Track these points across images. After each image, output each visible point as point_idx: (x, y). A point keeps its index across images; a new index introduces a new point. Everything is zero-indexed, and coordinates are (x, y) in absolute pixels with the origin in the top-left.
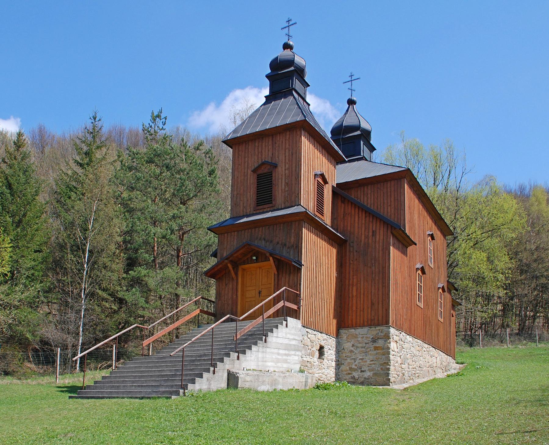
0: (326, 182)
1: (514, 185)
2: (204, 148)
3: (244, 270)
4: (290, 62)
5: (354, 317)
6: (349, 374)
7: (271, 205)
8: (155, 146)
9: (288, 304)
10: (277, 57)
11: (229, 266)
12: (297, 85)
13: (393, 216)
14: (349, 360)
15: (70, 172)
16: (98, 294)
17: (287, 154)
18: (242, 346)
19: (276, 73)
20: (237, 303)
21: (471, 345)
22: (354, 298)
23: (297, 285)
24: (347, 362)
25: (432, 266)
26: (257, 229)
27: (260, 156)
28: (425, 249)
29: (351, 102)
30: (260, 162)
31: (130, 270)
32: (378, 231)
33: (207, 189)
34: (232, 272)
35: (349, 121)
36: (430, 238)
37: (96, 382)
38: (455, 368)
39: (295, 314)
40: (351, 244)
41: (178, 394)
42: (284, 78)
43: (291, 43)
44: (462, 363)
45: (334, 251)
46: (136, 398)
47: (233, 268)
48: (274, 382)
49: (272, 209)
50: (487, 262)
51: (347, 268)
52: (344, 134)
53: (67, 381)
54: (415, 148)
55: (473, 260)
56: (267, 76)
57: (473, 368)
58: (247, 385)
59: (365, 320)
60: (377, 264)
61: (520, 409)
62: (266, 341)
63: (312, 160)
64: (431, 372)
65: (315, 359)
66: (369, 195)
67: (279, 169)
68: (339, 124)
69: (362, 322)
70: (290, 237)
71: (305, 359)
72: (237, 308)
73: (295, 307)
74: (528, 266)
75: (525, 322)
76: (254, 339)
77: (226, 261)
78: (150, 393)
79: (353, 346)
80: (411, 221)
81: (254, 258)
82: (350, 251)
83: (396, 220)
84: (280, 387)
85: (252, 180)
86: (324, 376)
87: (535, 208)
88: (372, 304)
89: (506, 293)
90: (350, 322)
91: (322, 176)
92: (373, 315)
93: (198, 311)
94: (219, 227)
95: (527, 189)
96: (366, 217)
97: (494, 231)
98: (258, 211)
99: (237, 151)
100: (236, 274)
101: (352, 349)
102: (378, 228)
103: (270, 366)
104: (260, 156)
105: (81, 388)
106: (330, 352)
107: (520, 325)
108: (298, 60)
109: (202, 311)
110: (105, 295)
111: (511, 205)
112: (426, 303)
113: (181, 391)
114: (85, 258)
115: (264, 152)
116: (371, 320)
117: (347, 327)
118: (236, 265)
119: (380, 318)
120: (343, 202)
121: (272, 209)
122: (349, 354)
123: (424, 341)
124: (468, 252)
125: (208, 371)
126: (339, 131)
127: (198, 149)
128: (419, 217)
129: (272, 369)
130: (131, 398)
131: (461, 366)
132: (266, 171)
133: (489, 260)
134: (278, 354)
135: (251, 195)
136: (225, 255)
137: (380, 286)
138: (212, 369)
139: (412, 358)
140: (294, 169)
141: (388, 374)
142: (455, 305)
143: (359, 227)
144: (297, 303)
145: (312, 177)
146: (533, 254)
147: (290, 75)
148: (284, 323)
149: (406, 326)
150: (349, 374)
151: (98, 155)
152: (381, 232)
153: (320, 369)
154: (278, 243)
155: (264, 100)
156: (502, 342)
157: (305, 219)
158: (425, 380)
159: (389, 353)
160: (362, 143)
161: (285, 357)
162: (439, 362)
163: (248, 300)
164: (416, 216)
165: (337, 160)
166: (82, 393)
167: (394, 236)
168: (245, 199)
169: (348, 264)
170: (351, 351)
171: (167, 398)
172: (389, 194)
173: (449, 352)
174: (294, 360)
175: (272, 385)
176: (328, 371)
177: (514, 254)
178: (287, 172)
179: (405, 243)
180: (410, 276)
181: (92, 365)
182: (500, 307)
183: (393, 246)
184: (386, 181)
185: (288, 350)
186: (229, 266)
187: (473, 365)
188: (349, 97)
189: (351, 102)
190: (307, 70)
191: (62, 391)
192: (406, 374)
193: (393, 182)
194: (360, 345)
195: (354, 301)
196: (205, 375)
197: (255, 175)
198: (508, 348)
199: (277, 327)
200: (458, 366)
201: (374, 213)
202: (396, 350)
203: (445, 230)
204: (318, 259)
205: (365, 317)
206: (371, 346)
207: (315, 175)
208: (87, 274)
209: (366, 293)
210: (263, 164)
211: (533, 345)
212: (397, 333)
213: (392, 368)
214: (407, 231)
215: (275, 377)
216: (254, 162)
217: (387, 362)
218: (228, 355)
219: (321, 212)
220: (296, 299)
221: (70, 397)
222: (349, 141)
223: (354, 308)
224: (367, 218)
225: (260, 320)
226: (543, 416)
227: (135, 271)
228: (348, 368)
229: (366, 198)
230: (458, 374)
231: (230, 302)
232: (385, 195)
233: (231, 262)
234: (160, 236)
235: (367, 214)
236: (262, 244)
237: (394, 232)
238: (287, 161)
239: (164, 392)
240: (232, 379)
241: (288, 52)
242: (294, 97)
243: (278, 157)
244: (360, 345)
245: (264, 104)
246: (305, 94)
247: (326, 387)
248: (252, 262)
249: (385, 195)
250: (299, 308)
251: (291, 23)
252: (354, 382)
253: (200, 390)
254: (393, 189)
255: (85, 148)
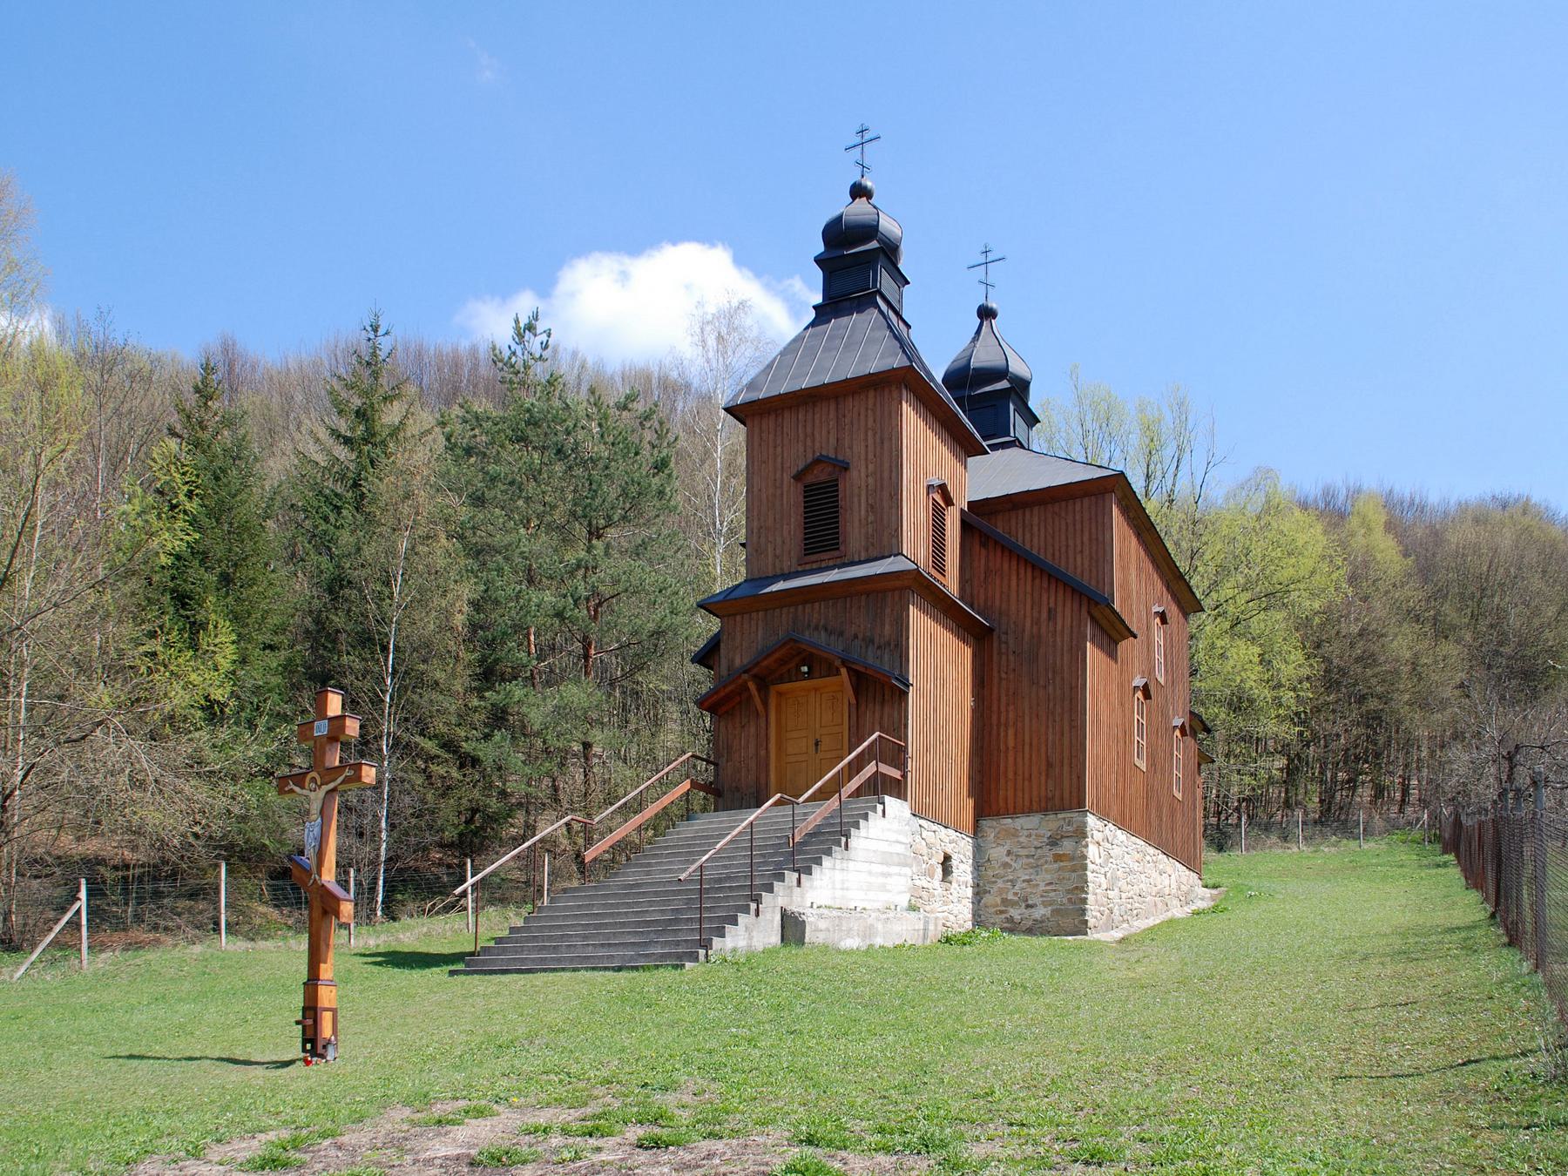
0: (949, 501)
1: (1311, 487)
2: (640, 407)
3: (780, 694)
4: (869, 230)
5: (1010, 793)
6: (1002, 912)
7: (836, 553)
8: (529, 401)
9: (886, 769)
10: (840, 217)
11: (752, 686)
12: (886, 282)
13: (1086, 575)
14: (1000, 884)
15: (321, 459)
16: (417, 745)
17: (870, 441)
18: (802, 855)
19: (837, 253)
20: (767, 765)
21: (1220, 849)
22: (1011, 753)
23: (900, 728)
24: (995, 888)
25: (1162, 680)
26: (808, 606)
27: (809, 443)
28: (1149, 643)
29: (986, 313)
30: (810, 460)
31: (488, 689)
32: (1059, 609)
33: (650, 506)
34: (757, 700)
35: (984, 358)
36: (1158, 620)
37: (499, 940)
38: (1203, 898)
39: (898, 788)
40: (1003, 638)
41: (696, 959)
42: (855, 265)
43: (869, 184)
44: (1215, 887)
45: (968, 652)
46: (606, 969)
47: (759, 690)
48: (869, 931)
49: (839, 561)
50: (1257, 662)
51: (995, 690)
52: (972, 388)
53: (372, 942)
54: (1103, 407)
55: (1231, 662)
56: (818, 260)
57: (1241, 897)
58: (820, 938)
59: (1035, 799)
60: (1058, 679)
61: (1373, 969)
62: (847, 848)
63: (922, 452)
64: (1160, 905)
65: (937, 881)
66: (1035, 529)
67: (854, 473)
68: (963, 362)
69: (1027, 803)
70: (883, 625)
71: (918, 883)
72: (767, 776)
73: (896, 774)
74: (1343, 672)
75: (1333, 797)
76: (822, 842)
77: (745, 676)
78: (632, 958)
79: (1009, 853)
80: (1125, 584)
81: (805, 669)
82: (1000, 653)
83: (1093, 583)
84: (878, 941)
85: (793, 497)
86: (952, 918)
87: (1359, 541)
88: (1049, 765)
89: (1301, 734)
90: (1001, 803)
91: (943, 489)
92: (1050, 787)
93: (686, 785)
94: (724, 600)
95: (1341, 498)
96: (1033, 579)
97: (1272, 598)
98: (808, 567)
99: (757, 430)
100: (765, 704)
101: (1008, 859)
102: (1060, 603)
103: (856, 899)
104: (809, 443)
105: (472, 954)
106: (962, 867)
107: (1321, 801)
108: (887, 225)
109: (694, 784)
110: (430, 746)
111: (1313, 537)
112: (1152, 763)
113: (702, 952)
114: (386, 660)
115: (821, 433)
116: (1048, 799)
117: (998, 814)
118: (764, 683)
119: (1066, 795)
120: (983, 545)
121: (839, 561)
122: (1001, 871)
123: (1148, 840)
124: (1219, 643)
125: (746, 910)
126: (961, 377)
127: (625, 408)
128: (1138, 575)
129: (860, 905)
130: (593, 969)
131: (1214, 892)
132: (823, 478)
133: (1264, 661)
134: (870, 873)
135: (791, 530)
136: (737, 662)
137: (1066, 728)
138: (753, 906)
139: (1131, 877)
140: (886, 474)
141: (1084, 911)
142: (1204, 758)
143: (1018, 598)
144: (901, 764)
145: (923, 491)
146: (1352, 645)
147: (869, 259)
148: (880, 807)
149: (1115, 810)
150: (1002, 912)
151: (390, 415)
152: (1067, 612)
153: (945, 903)
154: (856, 636)
155: (812, 315)
156: (1285, 839)
157: (918, 586)
158: (1151, 922)
159: (1085, 868)
160: (1012, 407)
161: (881, 880)
162: (1174, 885)
163: (792, 759)
164: (1133, 573)
165: (966, 447)
166: (476, 963)
167: (1093, 619)
168: (779, 540)
169: (996, 681)
170: (1006, 865)
171: (676, 967)
172: (1078, 526)
173: (1192, 863)
174: (898, 890)
175: (864, 938)
176: (960, 907)
177: (1315, 646)
178: (871, 480)
179: (1113, 632)
180: (1122, 705)
181: (411, 906)
182: (1281, 762)
183: (1093, 642)
184: (1074, 498)
185: (887, 864)
186: (752, 686)
187: (1238, 889)
188: (982, 301)
189: (986, 313)
190: (903, 247)
191: (379, 964)
192: (1116, 911)
193: (1086, 501)
194: (1023, 852)
195: (1011, 759)
196: (742, 918)
197: (800, 487)
198: (1298, 851)
199: (866, 817)
200: (1208, 892)
201: (1053, 568)
202: (1098, 861)
203: (1188, 603)
204: (937, 666)
205: (1035, 793)
206: (1049, 854)
207: (929, 487)
208: (392, 699)
209: (1035, 742)
210: (818, 461)
211: (1353, 844)
212: (1100, 824)
213: (1091, 897)
214: (1116, 606)
215: (870, 921)
216: (796, 456)
217: (1081, 887)
218: (781, 878)
219: (941, 570)
220: (898, 756)
221: (452, 973)
222: (985, 404)
223: (1011, 775)
224: (1037, 581)
225: (833, 803)
226: (1420, 979)
227: (498, 693)
228: (998, 900)
229: (1028, 536)
230: (1214, 910)
231: (753, 765)
232: (1071, 528)
233: (755, 677)
234: (551, 612)
235: (1037, 573)
236: (822, 638)
237: (1096, 614)
238: (871, 456)
239: (663, 956)
240: (792, 927)
241: (861, 203)
242: (881, 312)
243: (851, 448)
244: (1023, 852)
245: (813, 324)
246: (900, 302)
247: (963, 940)
248: (800, 677)
249: (1071, 528)
250: (904, 776)
251: (867, 136)
252: (1012, 928)
253: (734, 950)
254: (1086, 515)
255: (357, 402)
